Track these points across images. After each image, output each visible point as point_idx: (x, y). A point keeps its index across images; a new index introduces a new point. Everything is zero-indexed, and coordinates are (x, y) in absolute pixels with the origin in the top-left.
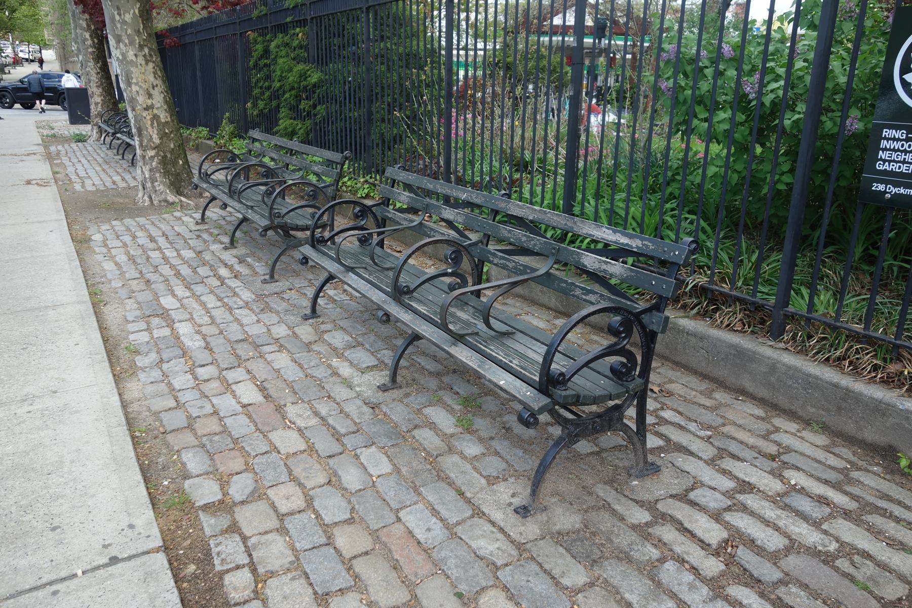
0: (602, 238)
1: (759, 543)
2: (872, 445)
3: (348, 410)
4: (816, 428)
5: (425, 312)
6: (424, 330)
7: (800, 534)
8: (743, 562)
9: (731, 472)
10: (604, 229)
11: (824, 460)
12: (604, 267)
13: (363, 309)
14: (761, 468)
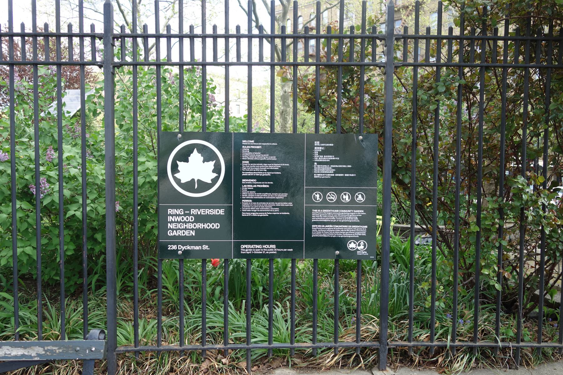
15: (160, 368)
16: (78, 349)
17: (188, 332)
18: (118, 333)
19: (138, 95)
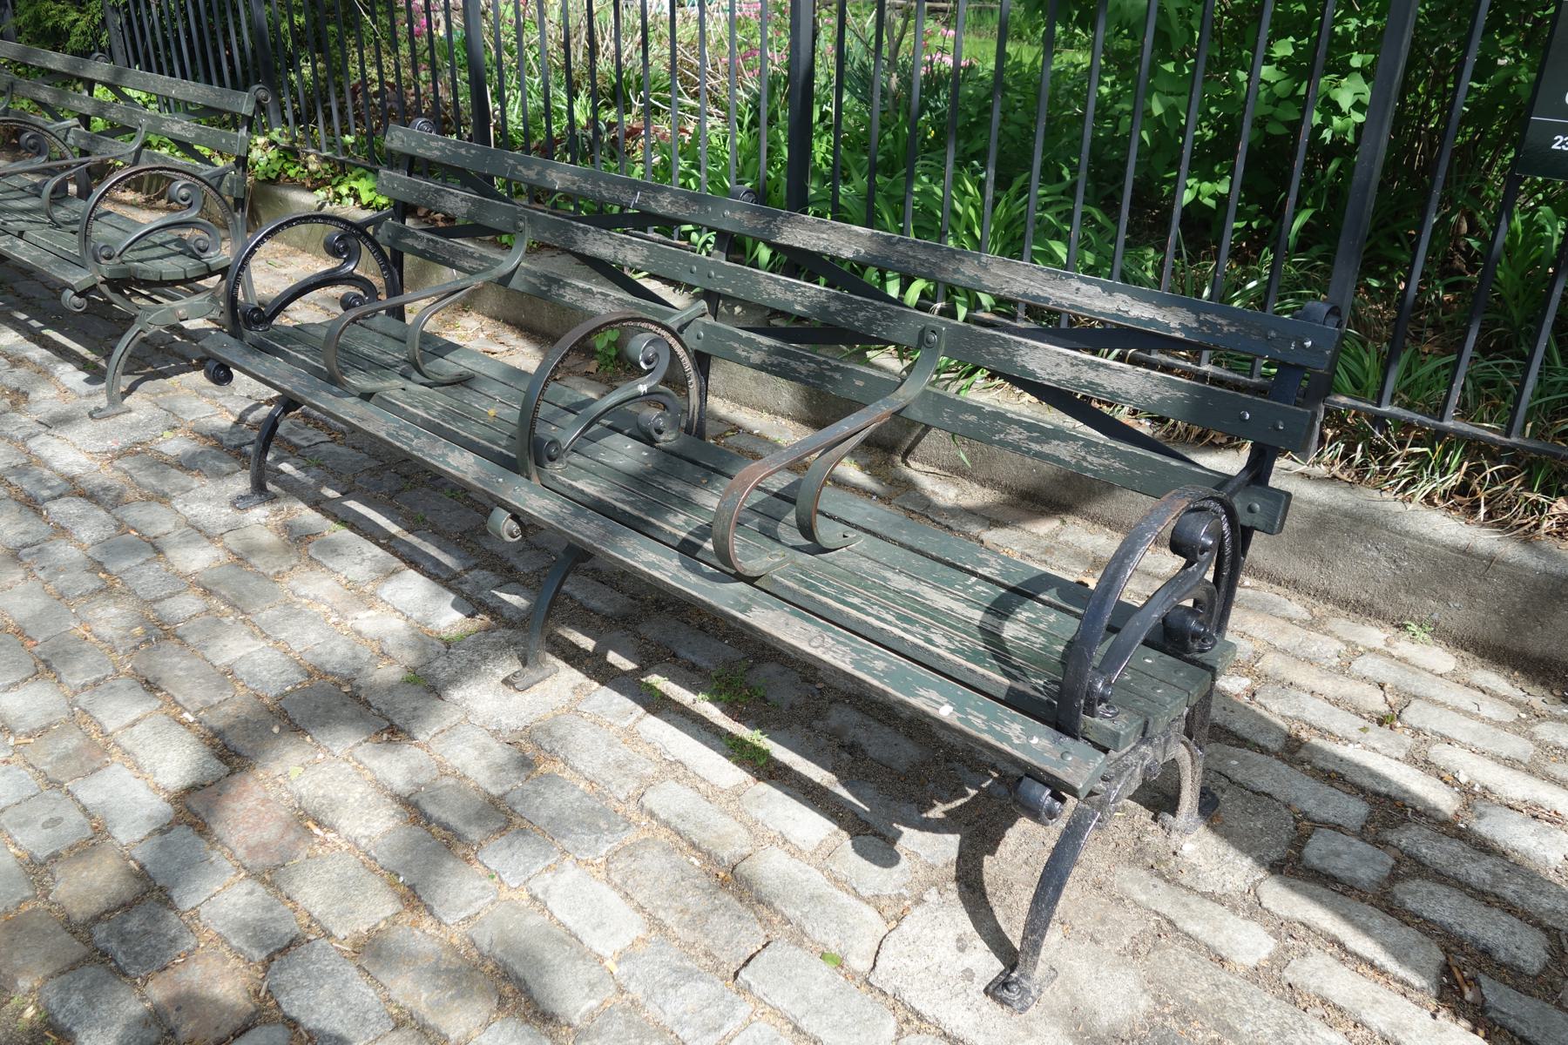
0: (1072, 306)
1: (1502, 955)
2: (1541, 660)
3: (457, 763)
4: (1421, 635)
5: (627, 508)
6: (651, 565)
7: (1555, 911)
8: (1512, 1022)
9: (1343, 776)
10: (1076, 284)
11: (1474, 709)
12: (1089, 375)
13: (373, 464)
14: (1387, 751)
15: (1432, 474)
16: (1273, 334)
17: (1539, 410)
18: (1340, 369)
19: (148, 1005)
